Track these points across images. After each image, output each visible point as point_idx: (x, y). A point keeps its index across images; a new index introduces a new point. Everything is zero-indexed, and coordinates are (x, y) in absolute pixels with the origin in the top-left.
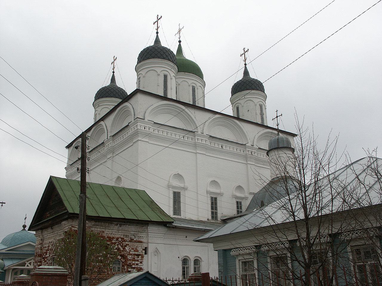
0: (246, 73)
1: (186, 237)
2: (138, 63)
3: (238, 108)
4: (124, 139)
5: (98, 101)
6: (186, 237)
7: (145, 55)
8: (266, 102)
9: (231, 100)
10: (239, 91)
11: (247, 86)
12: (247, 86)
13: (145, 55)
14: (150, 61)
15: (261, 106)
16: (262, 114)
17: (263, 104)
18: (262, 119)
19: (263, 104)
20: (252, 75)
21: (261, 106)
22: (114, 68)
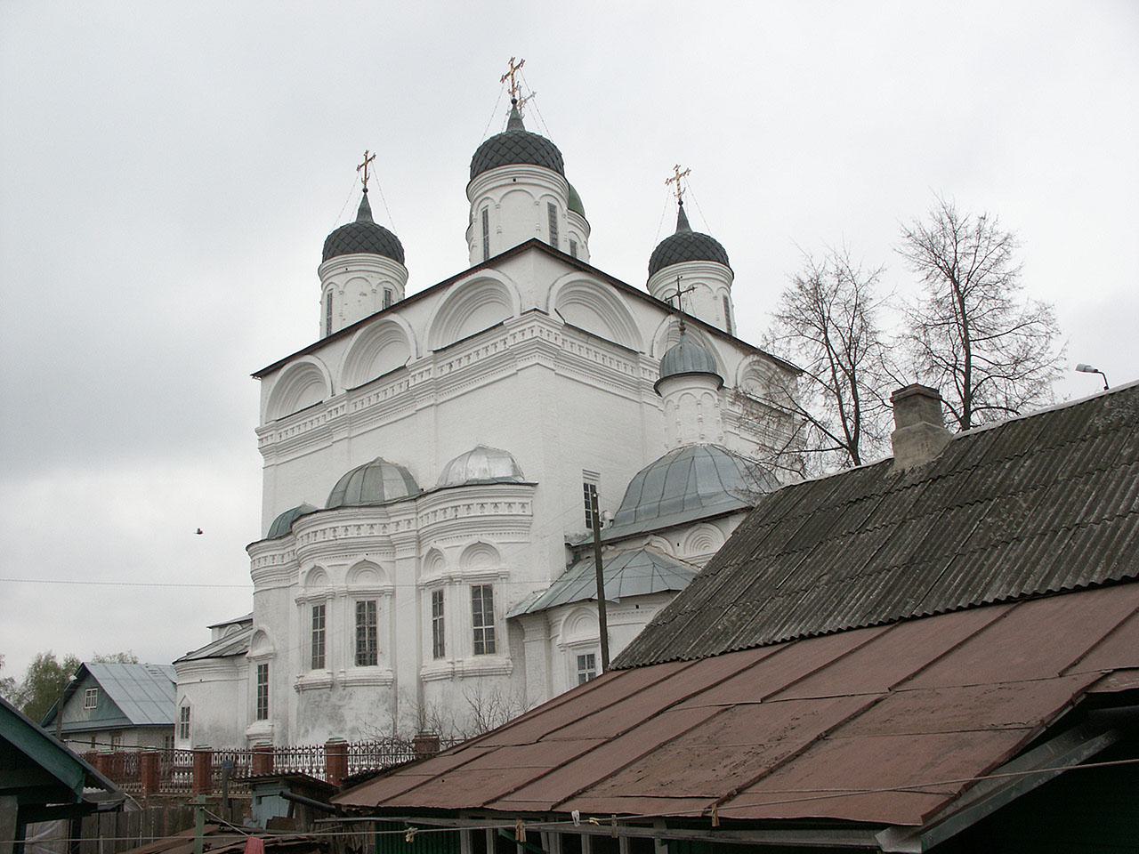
0: (682, 221)
1: (637, 607)
2: (472, 178)
3: (330, 297)
4: (453, 370)
5: (657, 276)
6: (637, 607)
7: (489, 157)
8: (731, 288)
9: (321, 272)
10: (343, 252)
11: (687, 248)
12: (687, 248)
13: (489, 157)
14: (495, 173)
15: (726, 300)
16: (728, 321)
17: (394, 289)
18: (729, 329)
19: (392, 287)
20: (379, 218)
21: (726, 300)
22: (366, 179)
